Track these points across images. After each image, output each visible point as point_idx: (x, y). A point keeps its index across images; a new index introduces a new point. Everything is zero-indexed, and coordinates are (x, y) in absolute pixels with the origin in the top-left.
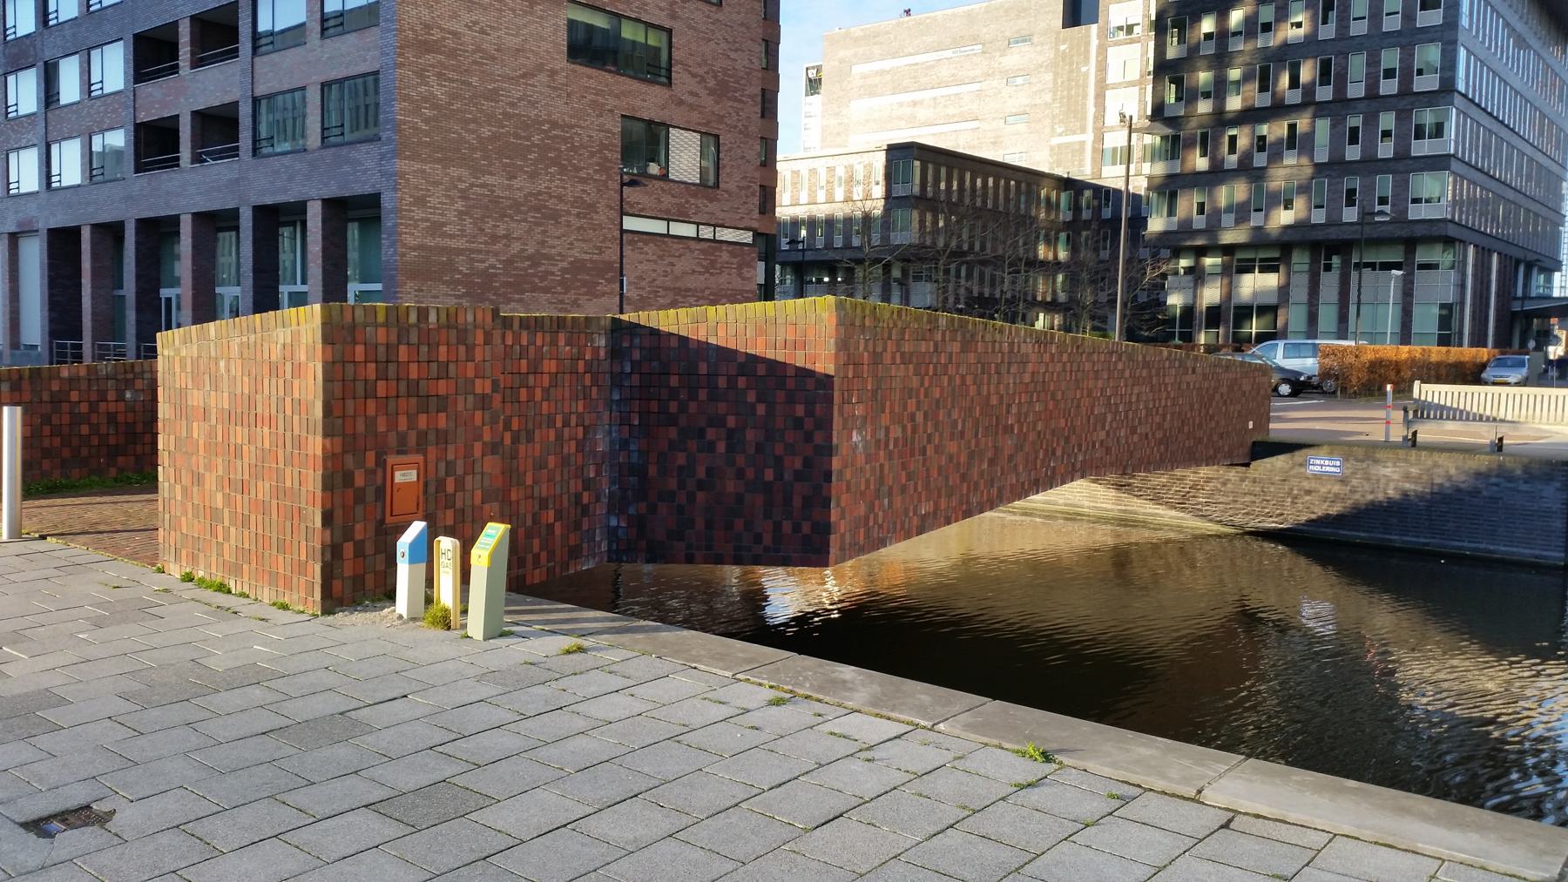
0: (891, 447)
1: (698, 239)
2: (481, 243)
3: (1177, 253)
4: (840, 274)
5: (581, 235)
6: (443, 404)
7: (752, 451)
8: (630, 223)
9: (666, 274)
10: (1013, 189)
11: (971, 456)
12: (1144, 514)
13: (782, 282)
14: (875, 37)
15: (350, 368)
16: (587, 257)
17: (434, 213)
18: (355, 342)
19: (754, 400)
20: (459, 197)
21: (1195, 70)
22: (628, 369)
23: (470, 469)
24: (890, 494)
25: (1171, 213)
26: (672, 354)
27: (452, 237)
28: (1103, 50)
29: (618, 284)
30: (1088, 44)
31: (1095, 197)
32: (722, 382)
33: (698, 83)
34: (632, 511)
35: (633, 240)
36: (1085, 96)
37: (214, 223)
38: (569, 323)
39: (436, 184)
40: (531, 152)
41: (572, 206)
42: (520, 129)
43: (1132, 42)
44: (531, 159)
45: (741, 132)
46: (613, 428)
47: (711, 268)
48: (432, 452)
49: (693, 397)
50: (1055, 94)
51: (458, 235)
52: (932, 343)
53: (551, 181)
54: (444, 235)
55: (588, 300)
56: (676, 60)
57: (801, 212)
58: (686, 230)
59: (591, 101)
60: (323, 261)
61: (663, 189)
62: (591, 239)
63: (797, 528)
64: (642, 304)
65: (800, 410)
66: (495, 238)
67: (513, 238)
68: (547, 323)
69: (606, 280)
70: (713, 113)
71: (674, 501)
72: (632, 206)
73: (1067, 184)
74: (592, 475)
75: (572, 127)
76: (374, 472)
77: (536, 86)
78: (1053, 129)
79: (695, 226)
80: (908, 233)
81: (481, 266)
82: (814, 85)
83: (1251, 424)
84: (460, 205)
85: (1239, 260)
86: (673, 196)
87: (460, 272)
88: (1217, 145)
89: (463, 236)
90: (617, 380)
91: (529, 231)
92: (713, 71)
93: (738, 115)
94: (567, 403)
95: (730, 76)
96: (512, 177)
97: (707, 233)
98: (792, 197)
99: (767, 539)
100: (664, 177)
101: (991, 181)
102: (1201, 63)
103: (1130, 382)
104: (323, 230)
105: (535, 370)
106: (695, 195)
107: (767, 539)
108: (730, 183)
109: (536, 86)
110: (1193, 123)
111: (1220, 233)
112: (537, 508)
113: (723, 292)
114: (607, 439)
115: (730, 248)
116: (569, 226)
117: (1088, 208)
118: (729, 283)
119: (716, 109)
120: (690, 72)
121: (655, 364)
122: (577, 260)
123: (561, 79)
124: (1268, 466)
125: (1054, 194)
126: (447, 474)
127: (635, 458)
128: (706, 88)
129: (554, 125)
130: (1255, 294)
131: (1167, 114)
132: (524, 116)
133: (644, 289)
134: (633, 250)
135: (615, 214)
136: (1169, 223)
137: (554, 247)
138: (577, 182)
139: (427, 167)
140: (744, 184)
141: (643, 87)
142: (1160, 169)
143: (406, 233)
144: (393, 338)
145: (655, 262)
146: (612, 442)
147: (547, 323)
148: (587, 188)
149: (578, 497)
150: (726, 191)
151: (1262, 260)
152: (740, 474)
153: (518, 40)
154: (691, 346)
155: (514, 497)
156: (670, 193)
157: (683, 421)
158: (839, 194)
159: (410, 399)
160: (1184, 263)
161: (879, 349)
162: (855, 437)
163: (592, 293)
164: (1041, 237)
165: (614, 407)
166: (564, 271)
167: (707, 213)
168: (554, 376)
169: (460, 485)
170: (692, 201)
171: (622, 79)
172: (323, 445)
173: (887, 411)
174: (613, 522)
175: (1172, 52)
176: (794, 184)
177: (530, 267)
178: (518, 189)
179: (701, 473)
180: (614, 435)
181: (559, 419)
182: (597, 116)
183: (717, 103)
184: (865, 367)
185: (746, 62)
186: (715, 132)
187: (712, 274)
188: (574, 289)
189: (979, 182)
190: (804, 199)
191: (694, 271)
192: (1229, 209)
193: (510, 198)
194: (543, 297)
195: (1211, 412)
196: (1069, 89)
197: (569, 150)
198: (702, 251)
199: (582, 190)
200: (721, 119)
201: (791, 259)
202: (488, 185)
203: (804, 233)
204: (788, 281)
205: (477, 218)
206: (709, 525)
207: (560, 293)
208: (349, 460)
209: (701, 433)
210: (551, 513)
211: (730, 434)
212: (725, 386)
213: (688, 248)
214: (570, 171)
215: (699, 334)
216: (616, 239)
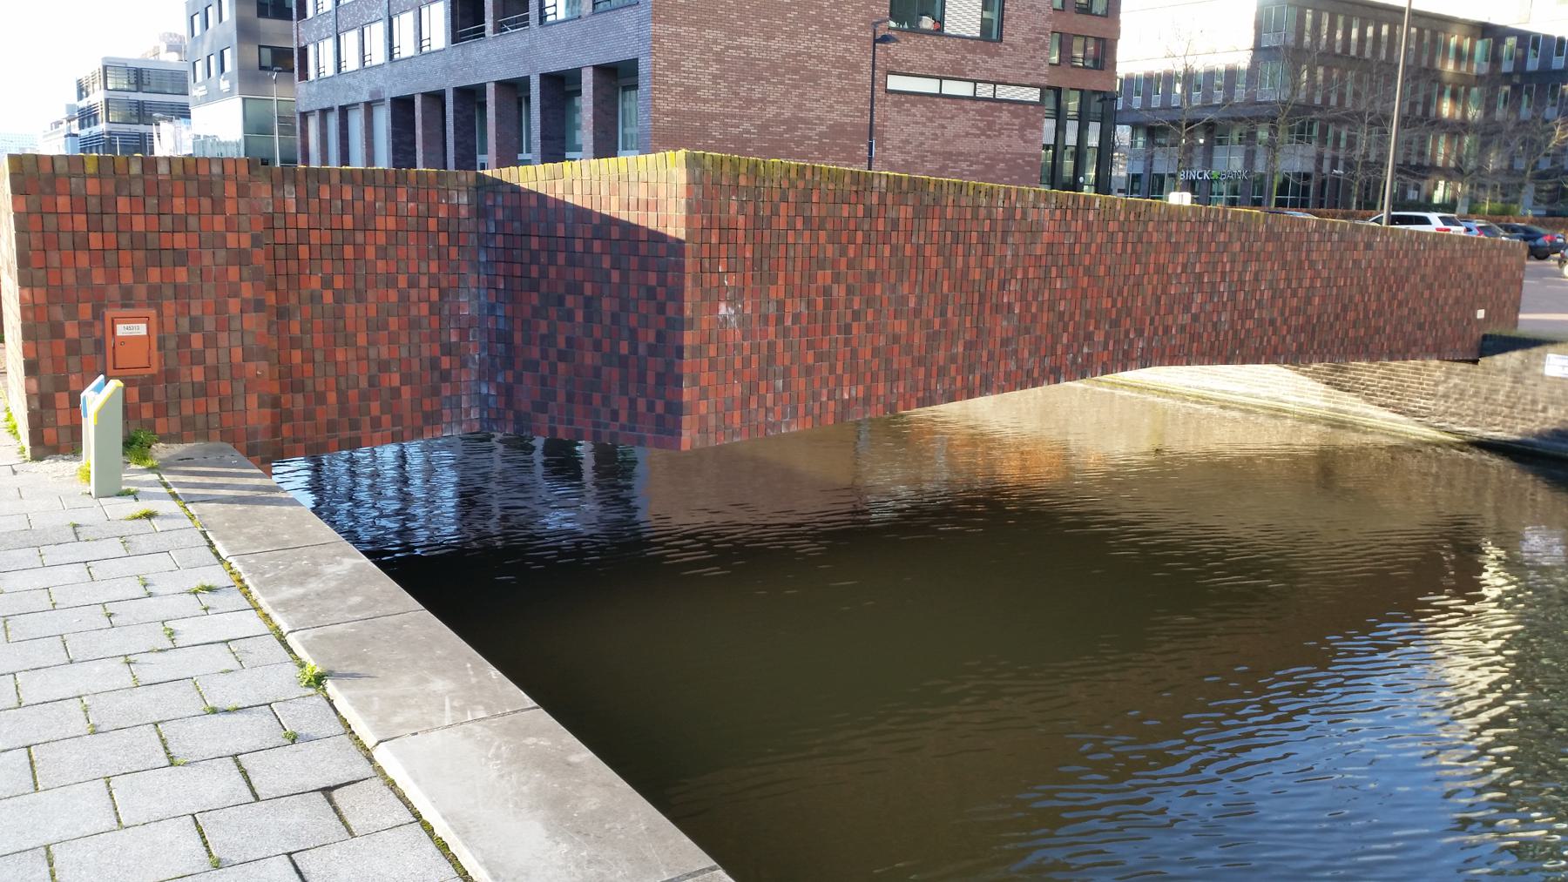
0: (788, 322)
1: (974, 99)
2: (735, 107)
5: (842, 97)
6: (181, 257)
7: (607, 320)
8: (895, 83)
11: (932, 337)
12: (1355, 414)
15: (51, 222)
16: (847, 120)
17: (688, 78)
18: (56, 194)
20: (714, 60)
22: (492, 230)
23: (223, 325)
24: (786, 374)
27: (705, 101)
31: (1519, 45)
32: (579, 246)
34: (500, 379)
37: (514, 89)
39: (691, 47)
40: (790, 10)
41: (834, 67)
46: (481, 292)
48: (170, 308)
49: (552, 261)
51: (712, 100)
54: (698, 100)
58: (964, 89)
60: (594, 128)
61: (935, 45)
63: (651, 407)
65: (652, 278)
66: (749, 102)
67: (770, 102)
74: (454, 339)
76: (91, 325)
79: (972, 84)
80: (1271, 92)
81: (735, 131)
83: (1481, 314)
84: (714, 68)
87: (713, 138)
89: (716, 101)
90: (484, 240)
96: (769, 38)
97: (985, 91)
99: (623, 416)
100: (939, 31)
101: (1385, 30)
103: (1240, 258)
104: (594, 97)
105: (364, 225)
106: (973, 51)
107: (623, 416)
108: (1015, 33)
113: (1001, 156)
114: (475, 303)
115: (1012, 108)
116: (829, 88)
118: (1010, 146)
121: (517, 224)
124: (1499, 364)
125: (1467, 43)
126: (192, 329)
134: (898, 112)
138: (840, 41)
139: (681, 30)
140: (1032, 36)
143: (659, 98)
144: (110, 188)
145: (924, 124)
146: (481, 307)
150: (1011, 45)
152: (597, 346)
154: (548, 206)
155: (340, 357)
157: (544, 288)
159: (136, 252)
164: (1448, 92)
165: (482, 270)
166: (822, 135)
168: (392, 236)
169: (211, 341)
170: (969, 56)
172: (21, 296)
174: (484, 390)
177: (786, 131)
179: (562, 343)
180: (482, 298)
184: (741, 233)
187: (989, 137)
188: (832, 154)
189: (1370, 31)
191: (968, 134)
195: (1401, 296)
198: (978, 112)
199: (844, 49)
202: (744, 46)
203: (1178, 88)
204: (1140, 144)
205: (732, 82)
206: (570, 399)
208: (58, 313)
209: (561, 301)
211: (588, 302)
215: (558, 192)
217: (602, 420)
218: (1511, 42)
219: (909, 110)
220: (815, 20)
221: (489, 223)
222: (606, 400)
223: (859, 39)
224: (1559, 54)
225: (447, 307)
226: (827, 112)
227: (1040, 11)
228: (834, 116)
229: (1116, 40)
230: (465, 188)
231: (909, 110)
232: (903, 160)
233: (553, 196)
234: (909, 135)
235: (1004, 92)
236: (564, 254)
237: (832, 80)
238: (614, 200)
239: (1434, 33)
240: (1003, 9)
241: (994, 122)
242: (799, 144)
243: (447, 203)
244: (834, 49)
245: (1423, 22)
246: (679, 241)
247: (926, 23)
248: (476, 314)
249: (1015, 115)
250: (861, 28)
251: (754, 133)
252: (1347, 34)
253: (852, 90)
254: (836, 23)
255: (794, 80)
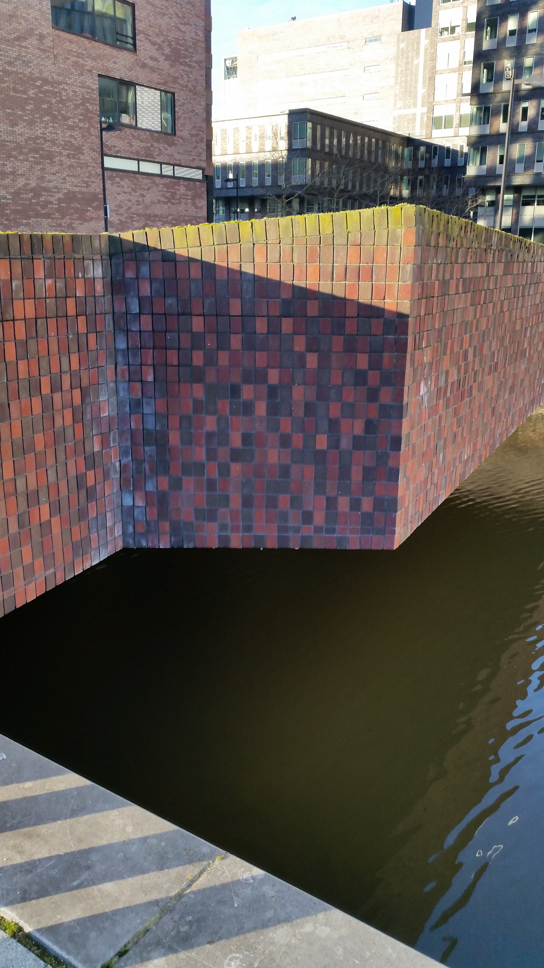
0: (448, 395)
1: (161, 176)
3: (484, 191)
4: (256, 206)
5: (72, 172)
7: (299, 412)
8: (109, 162)
9: (138, 203)
10: (373, 145)
13: (218, 212)
14: (273, 35)
16: (77, 189)
19: (303, 349)
21: (499, 58)
22: (135, 308)
25: (482, 162)
26: (193, 287)
28: (434, 45)
29: (102, 212)
30: (419, 43)
31: (427, 151)
32: (261, 326)
33: (158, 50)
34: (150, 487)
35: (112, 176)
36: (416, 82)
38: (48, 244)
41: (63, 149)
42: (18, 84)
43: (454, 39)
44: (28, 110)
45: (190, 91)
47: (172, 199)
50: (397, 79)
52: (486, 264)
53: (45, 128)
55: (80, 224)
56: (139, 31)
57: (229, 160)
59: (73, 62)
61: (133, 135)
62: (79, 175)
64: (123, 227)
67: (19, 175)
68: (15, 245)
69: (93, 208)
70: (169, 74)
71: (203, 474)
72: (110, 149)
73: (409, 141)
74: (97, 448)
75: (60, 83)
77: (28, 48)
78: (395, 104)
82: (231, 71)
85: (524, 197)
86: (141, 141)
88: (513, 115)
91: (31, 168)
92: (168, 40)
93: (188, 77)
94: (55, 360)
95: (182, 45)
97: (168, 170)
98: (222, 149)
99: (319, 518)
102: (505, 54)
106: (158, 141)
107: (319, 518)
108: (183, 131)
109: (28, 48)
110: (498, 98)
111: (513, 177)
112: (23, 507)
113: (182, 218)
114: (113, 400)
115: (186, 183)
116: (61, 165)
117: (422, 159)
119: (172, 71)
120: (150, 41)
121: (170, 301)
122: (69, 192)
123: (48, 42)
127: (150, 424)
128: (163, 54)
129: (45, 81)
130: (534, 220)
131: (482, 91)
132: (20, 73)
133: (122, 215)
134: (112, 184)
135: (98, 156)
136: (479, 170)
137: (51, 182)
138: (66, 129)
140: (194, 132)
141: (114, 52)
142: (474, 131)
145: (130, 194)
146: (120, 404)
147: (15, 245)
148: (75, 134)
149: (80, 480)
151: (540, 197)
152: (285, 441)
153: (11, 7)
154: (218, 277)
156: (138, 139)
157: (211, 376)
158: (255, 147)
160: (489, 198)
161: (447, 277)
162: (423, 390)
163: (83, 219)
165: (120, 359)
166: (60, 200)
167: (168, 155)
170: (156, 145)
171: (97, 44)
173: (448, 352)
174: (128, 501)
175: (486, 44)
176: (223, 139)
177: (33, 197)
178: (19, 134)
179: (236, 441)
180: (121, 394)
181: (45, 382)
182: (79, 75)
183: (172, 66)
185: (193, 34)
186: (172, 90)
187: (173, 204)
190: (230, 150)
191: (159, 201)
192: (520, 160)
193: (13, 142)
194: (45, 222)
196: (406, 76)
197: (58, 102)
198: (165, 185)
200: (175, 80)
201: (222, 195)
204: (221, 212)
206: (247, 502)
207: (59, 219)
209: (235, 391)
210: (45, 509)
211: (273, 391)
212: (265, 331)
213: (154, 182)
214: (60, 120)
216: (99, 175)
217: (290, 524)
218: (422, 149)
219: (119, 183)
220: (47, 112)
221: (129, 300)
222: (296, 502)
223: (81, 128)
224: (448, 157)
225: (89, 410)
226: (62, 183)
227: (198, 115)
228: (68, 186)
229: (212, 141)
230: (99, 257)
231: (119, 183)
232: (118, 220)
233: (224, 264)
234: (121, 201)
235: (181, 172)
236: (239, 337)
237: (63, 159)
238: (312, 267)
239: (384, 143)
240: (175, 112)
241: (175, 193)
242: (44, 206)
243: (83, 277)
244: (63, 136)
245: (378, 135)
246: (403, 317)
247: (125, 119)
248: (114, 413)
249: (188, 188)
250: (80, 120)
251: (9, 199)
252: (339, 141)
253: (78, 167)
254: (62, 115)
255: (36, 158)
